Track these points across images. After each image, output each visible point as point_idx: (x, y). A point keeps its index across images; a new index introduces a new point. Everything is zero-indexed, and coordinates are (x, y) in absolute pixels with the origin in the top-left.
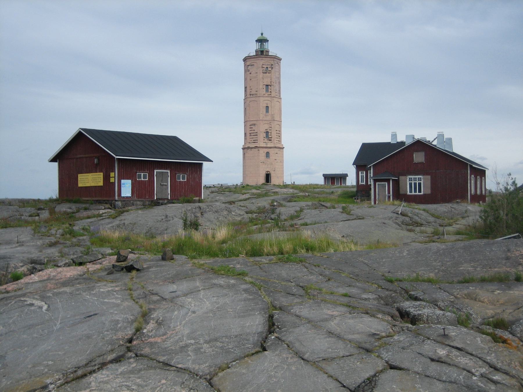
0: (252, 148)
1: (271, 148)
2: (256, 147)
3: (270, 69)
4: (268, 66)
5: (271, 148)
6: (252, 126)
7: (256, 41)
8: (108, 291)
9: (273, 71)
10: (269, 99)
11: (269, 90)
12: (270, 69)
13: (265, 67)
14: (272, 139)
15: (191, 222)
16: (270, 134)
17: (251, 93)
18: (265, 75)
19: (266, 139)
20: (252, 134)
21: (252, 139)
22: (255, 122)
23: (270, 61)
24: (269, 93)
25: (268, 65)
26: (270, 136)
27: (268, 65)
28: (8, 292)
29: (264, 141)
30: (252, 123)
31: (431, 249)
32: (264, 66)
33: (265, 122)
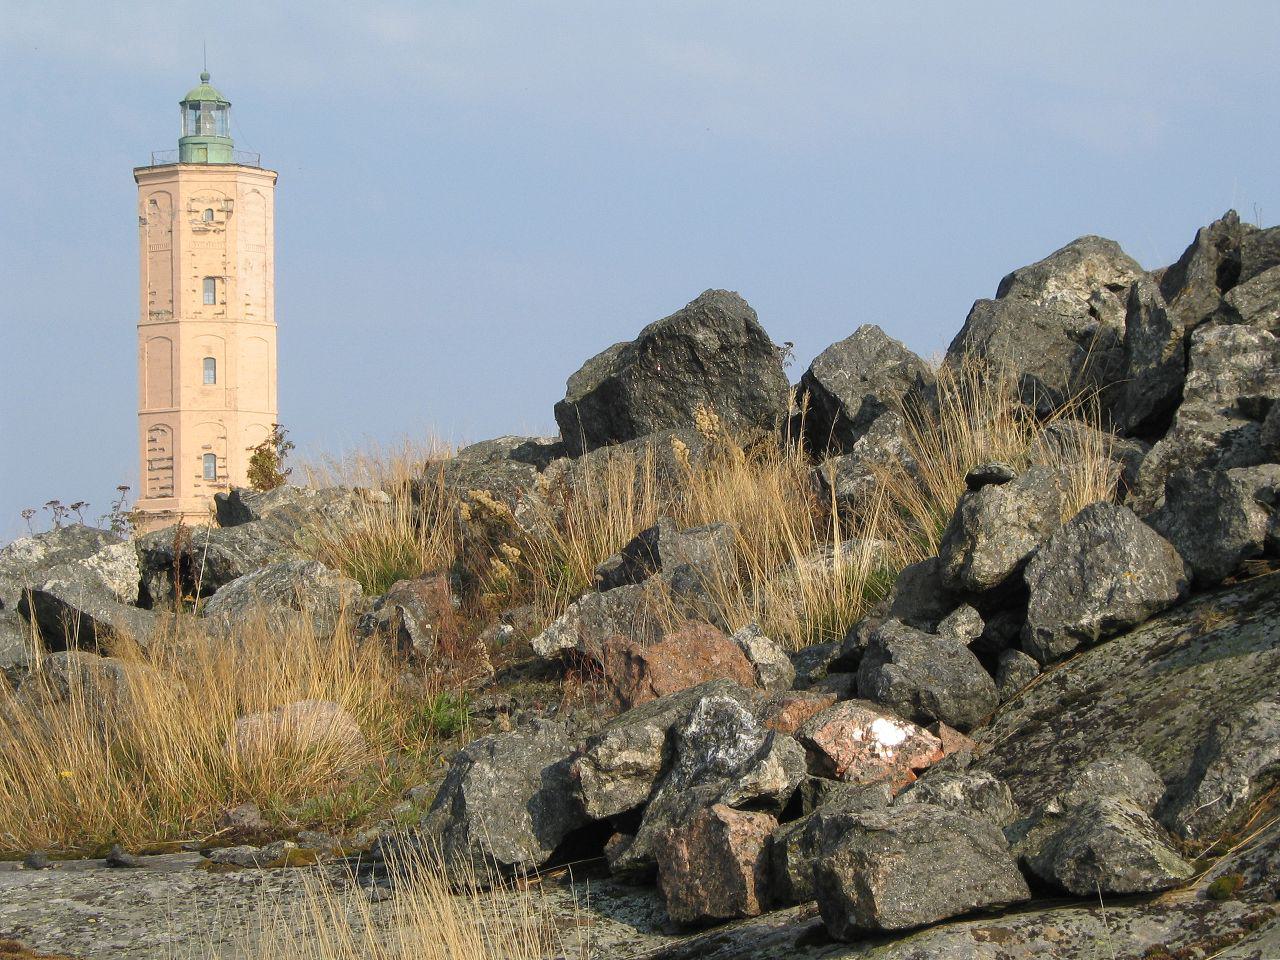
4: (215, 207)
6: (155, 435)
8: (1247, 822)
9: (231, 225)
11: (219, 299)
13: (202, 207)
16: (219, 463)
18: (200, 238)
19: (204, 484)
20: (156, 465)
21: (157, 484)
24: (219, 308)
25: (212, 201)
26: (220, 472)
27: (212, 201)
28: (160, 749)
29: (198, 491)
31: (732, 716)
32: (195, 206)
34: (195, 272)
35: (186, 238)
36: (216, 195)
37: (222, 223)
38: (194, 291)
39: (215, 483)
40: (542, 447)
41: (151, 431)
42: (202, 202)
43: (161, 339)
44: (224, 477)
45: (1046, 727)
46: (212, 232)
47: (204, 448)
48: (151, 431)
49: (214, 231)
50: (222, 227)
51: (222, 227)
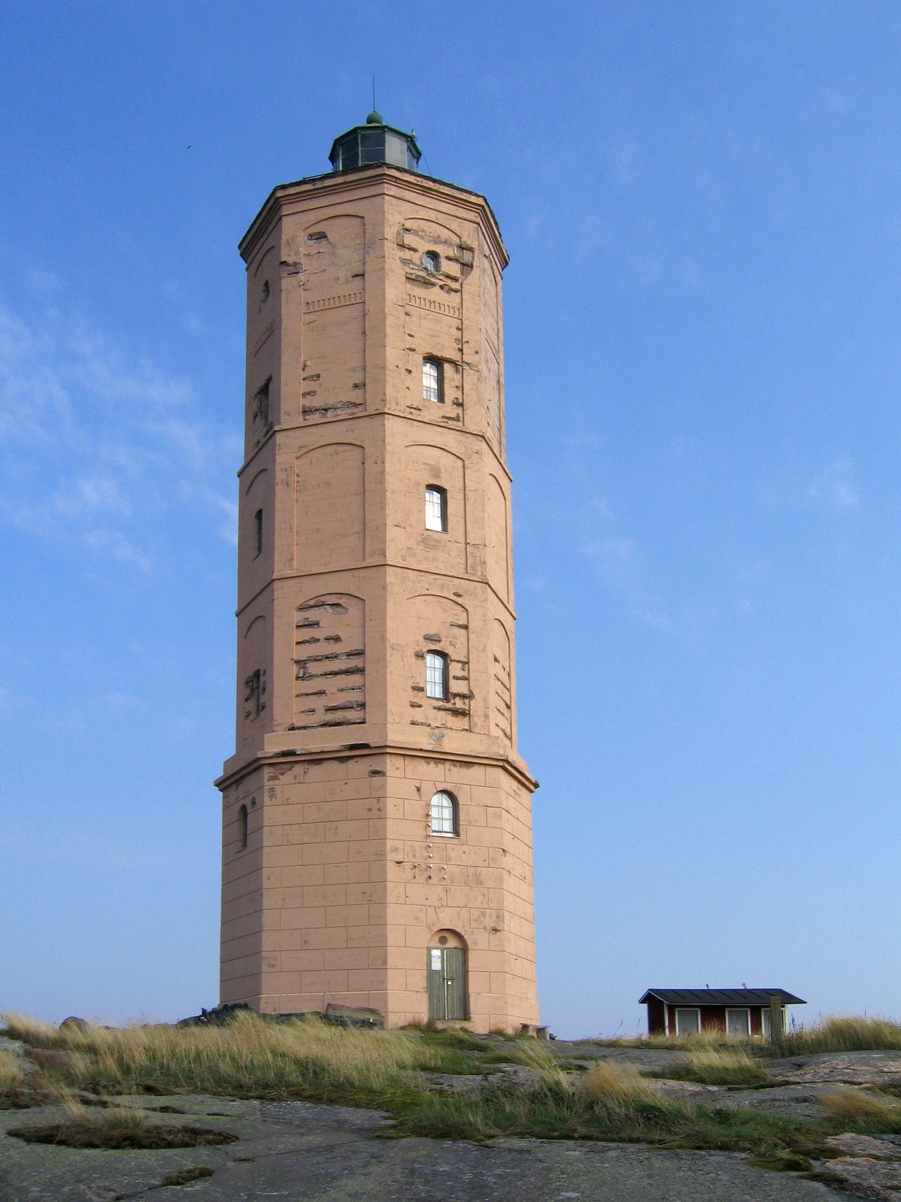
0: (316, 759)
1: (466, 762)
2: (359, 751)
3: (448, 267)
5: (466, 762)
6: (312, 615)
7: (424, 358)
10: (448, 439)
12: (454, 269)
14: (475, 706)
15: (401, 360)
17: (315, 402)
18: (419, 291)
20: (314, 668)
21: (319, 703)
22: (240, 855)
23: (455, 225)
24: (453, 411)
27: (437, 240)
30: (312, 589)
32: (409, 239)
33: (425, 583)
34: (409, 342)
35: (395, 288)
36: (445, 234)
37: (455, 279)
38: (410, 372)
39: (449, 706)
40: (214, 1011)
41: (302, 608)
42: (422, 237)
43: (331, 449)
44: (464, 697)
45: (521, 1092)
46: (438, 287)
47: (428, 638)
48: (302, 608)
49: (442, 287)
50: (455, 285)
51: (455, 285)
